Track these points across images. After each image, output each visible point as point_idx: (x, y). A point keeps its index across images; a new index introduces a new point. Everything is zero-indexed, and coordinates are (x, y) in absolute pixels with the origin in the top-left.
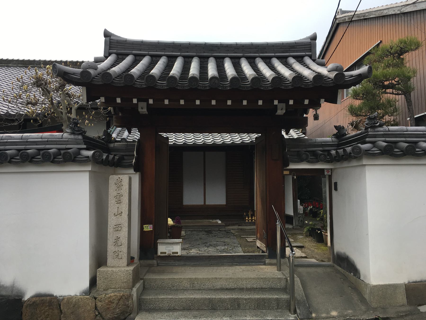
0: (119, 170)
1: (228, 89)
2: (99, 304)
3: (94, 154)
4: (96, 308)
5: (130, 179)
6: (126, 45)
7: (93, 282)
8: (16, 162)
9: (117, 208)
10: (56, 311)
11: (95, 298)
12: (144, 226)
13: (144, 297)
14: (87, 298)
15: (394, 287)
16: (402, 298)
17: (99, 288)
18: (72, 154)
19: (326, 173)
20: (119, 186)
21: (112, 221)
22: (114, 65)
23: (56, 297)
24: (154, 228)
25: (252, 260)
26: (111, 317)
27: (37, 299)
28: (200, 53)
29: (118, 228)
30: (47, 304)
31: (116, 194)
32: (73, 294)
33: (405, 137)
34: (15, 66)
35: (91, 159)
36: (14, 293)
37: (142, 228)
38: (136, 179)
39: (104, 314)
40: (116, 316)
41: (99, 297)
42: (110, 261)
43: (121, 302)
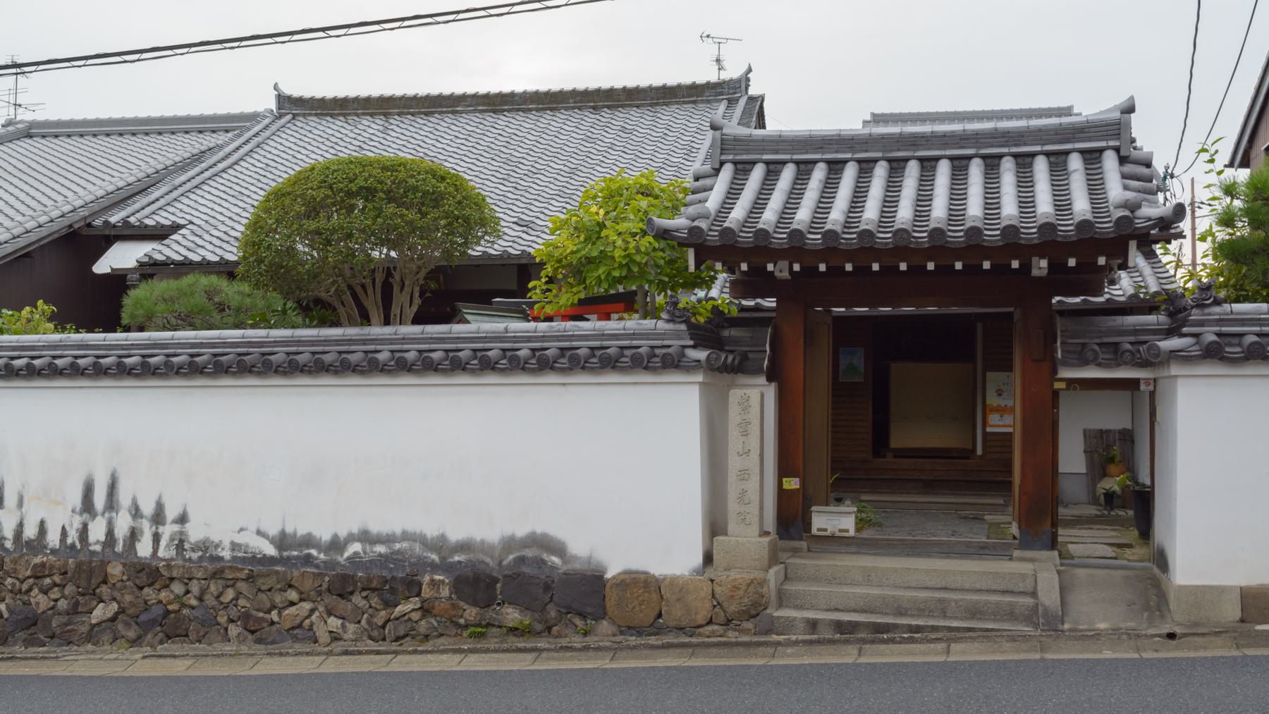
0: (742, 379)
2: (718, 589)
3: (708, 357)
5: (762, 395)
7: (708, 559)
8: (593, 368)
10: (655, 596)
11: (712, 581)
13: (787, 587)
15: (1221, 590)
16: (1232, 612)
19: (1143, 387)
20: (745, 405)
21: (734, 464)
22: (733, 193)
23: (654, 576)
24: (803, 483)
25: (987, 552)
29: (744, 475)
32: (678, 573)
33: (1261, 325)
34: (470, 112)
35: (704, 365)
37: (780, 484)
38: (771, 392)
39: (725, 605)
41: (717, 580)
42: (731, 527)
43: (751, 589)
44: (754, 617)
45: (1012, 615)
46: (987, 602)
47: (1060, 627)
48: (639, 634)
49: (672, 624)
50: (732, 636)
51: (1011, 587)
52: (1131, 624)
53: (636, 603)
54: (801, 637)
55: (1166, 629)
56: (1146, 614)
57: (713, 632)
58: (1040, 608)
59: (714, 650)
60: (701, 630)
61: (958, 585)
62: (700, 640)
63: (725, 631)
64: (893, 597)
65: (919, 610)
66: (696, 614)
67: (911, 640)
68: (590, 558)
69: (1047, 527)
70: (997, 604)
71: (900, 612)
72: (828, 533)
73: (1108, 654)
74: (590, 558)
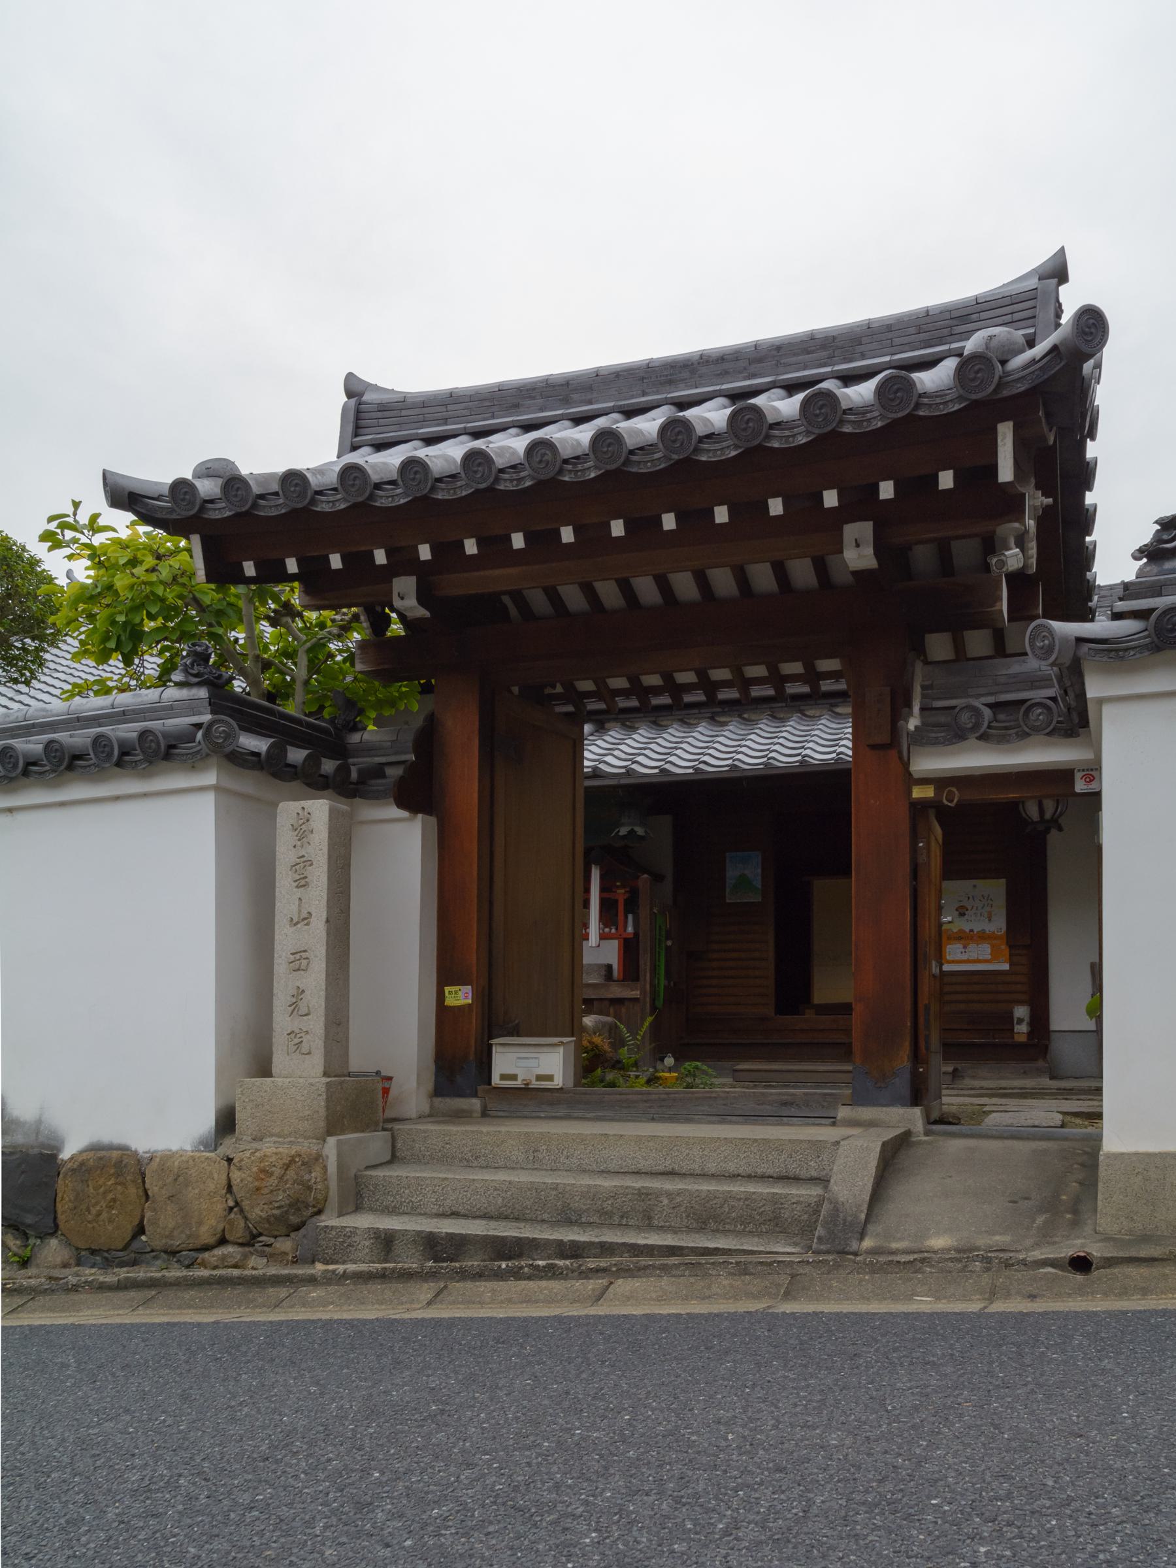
1: (593, 475)
2: (236, 1176)
4: (229, 1188)
6: (404, 413)
7: (226, 1123)
9: (297, 903)
10: (133, 1190)
11: (229, 1160)
12: (447, 989)
14: (207, 1158)
17: (240, 1133)
18: (160, 735)
20: (302, 832)
25: (793, 1111)
26: (264, 1215)
27: (91, 1154)
28: (632, 397)
30: (112, 1171)
31: (294, 860)
32: (174, 1148)
36: (41, 1139)
39: (245, 1204)
40: (276, 1212)
43: (291, 1174)
44: (297, 1228)
45: (774, 1222)
46: (730, 1196)
47: (854, 1246)
48: (108, 1264)
49: (158, 1244)
50: (258, 1266)
51: (794, 1169)
52: (1000, 1239)
53: (103, 1204)
54: (363, 1267)
55: (1069, 1249)
56: (1040, 1220)
57: (224, 1258)
58: (826, 1206)
59: (188, 1295)
60: (206, 1255)
61: (696, 1167)
62: (205, 1273)
63: (245, 1257)
64: (555, 1187)
65: (603, 1213)
66: (200, 1223)
67: (551, 1273)
68: (39, 1122)
69: (903, 1060)
70: (748, 1198)
71: (568, 1219)
72: (518, 1083)
73: (924, 1304)
74: (39, 1122)
